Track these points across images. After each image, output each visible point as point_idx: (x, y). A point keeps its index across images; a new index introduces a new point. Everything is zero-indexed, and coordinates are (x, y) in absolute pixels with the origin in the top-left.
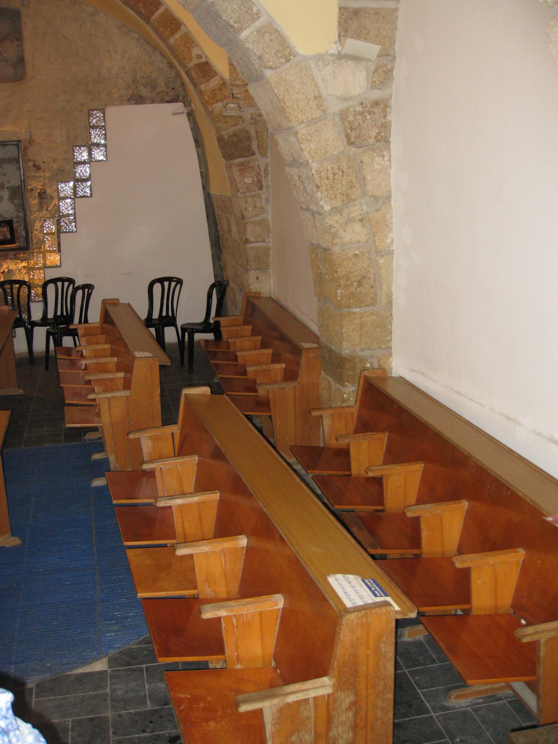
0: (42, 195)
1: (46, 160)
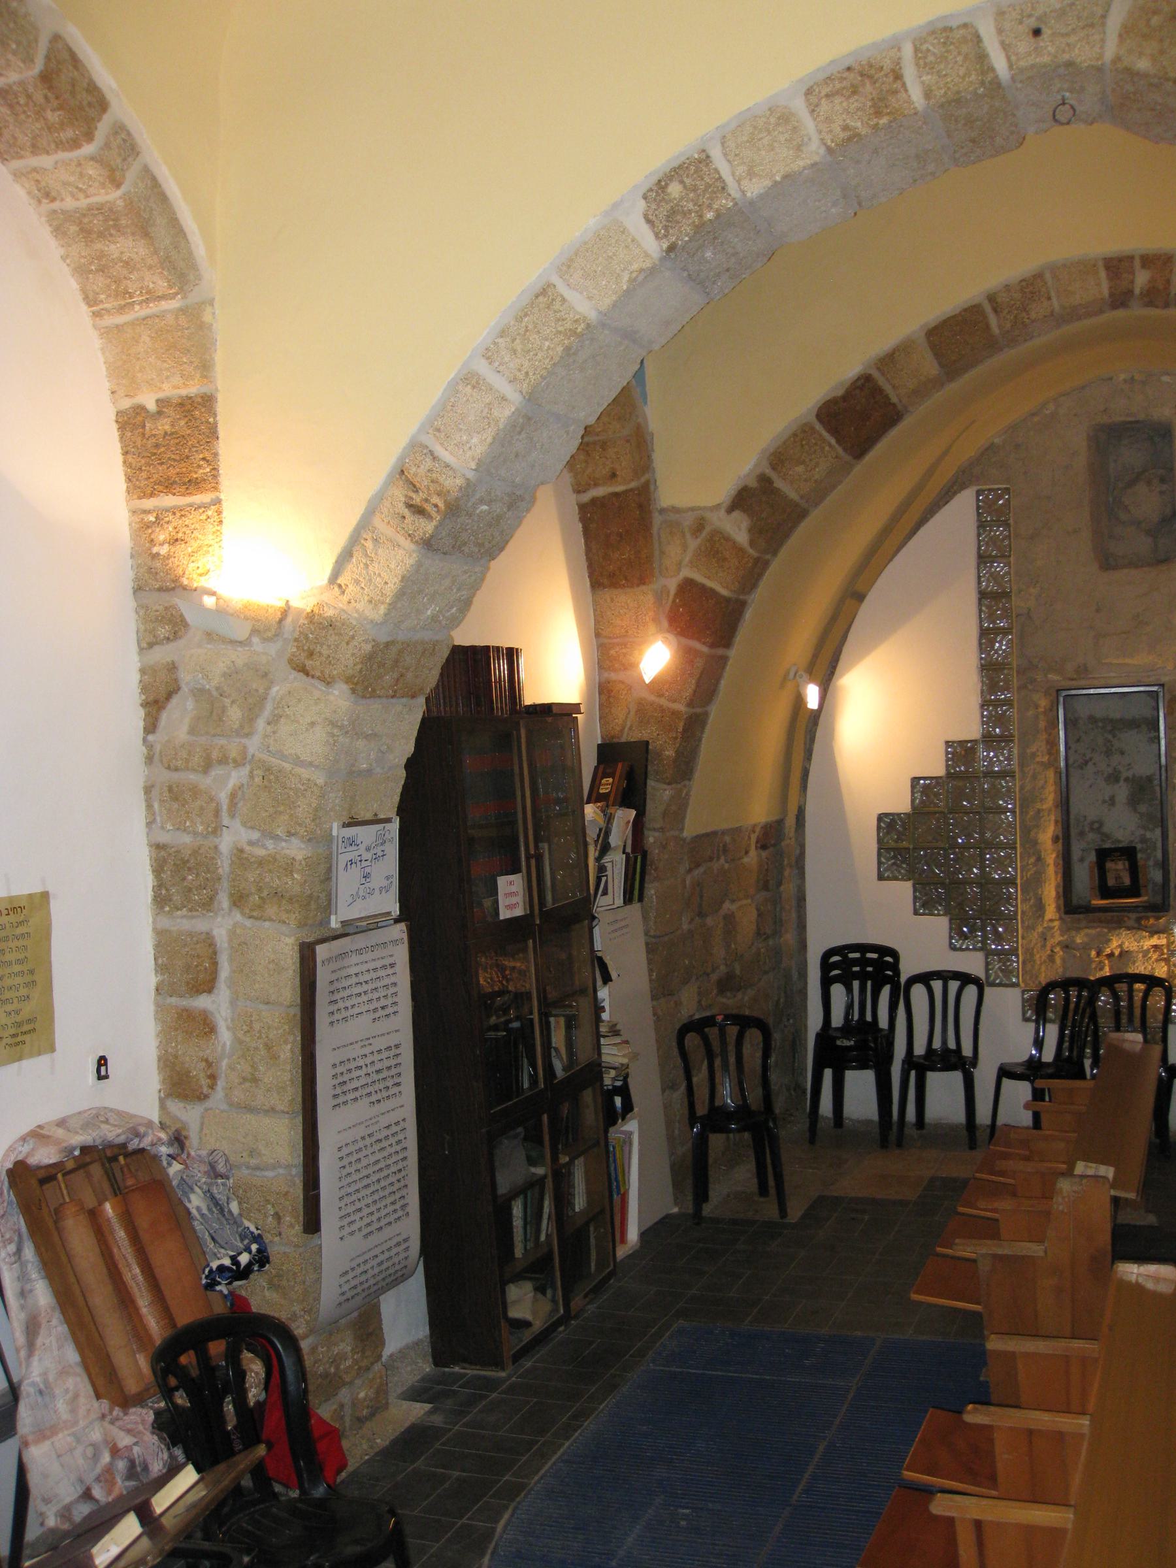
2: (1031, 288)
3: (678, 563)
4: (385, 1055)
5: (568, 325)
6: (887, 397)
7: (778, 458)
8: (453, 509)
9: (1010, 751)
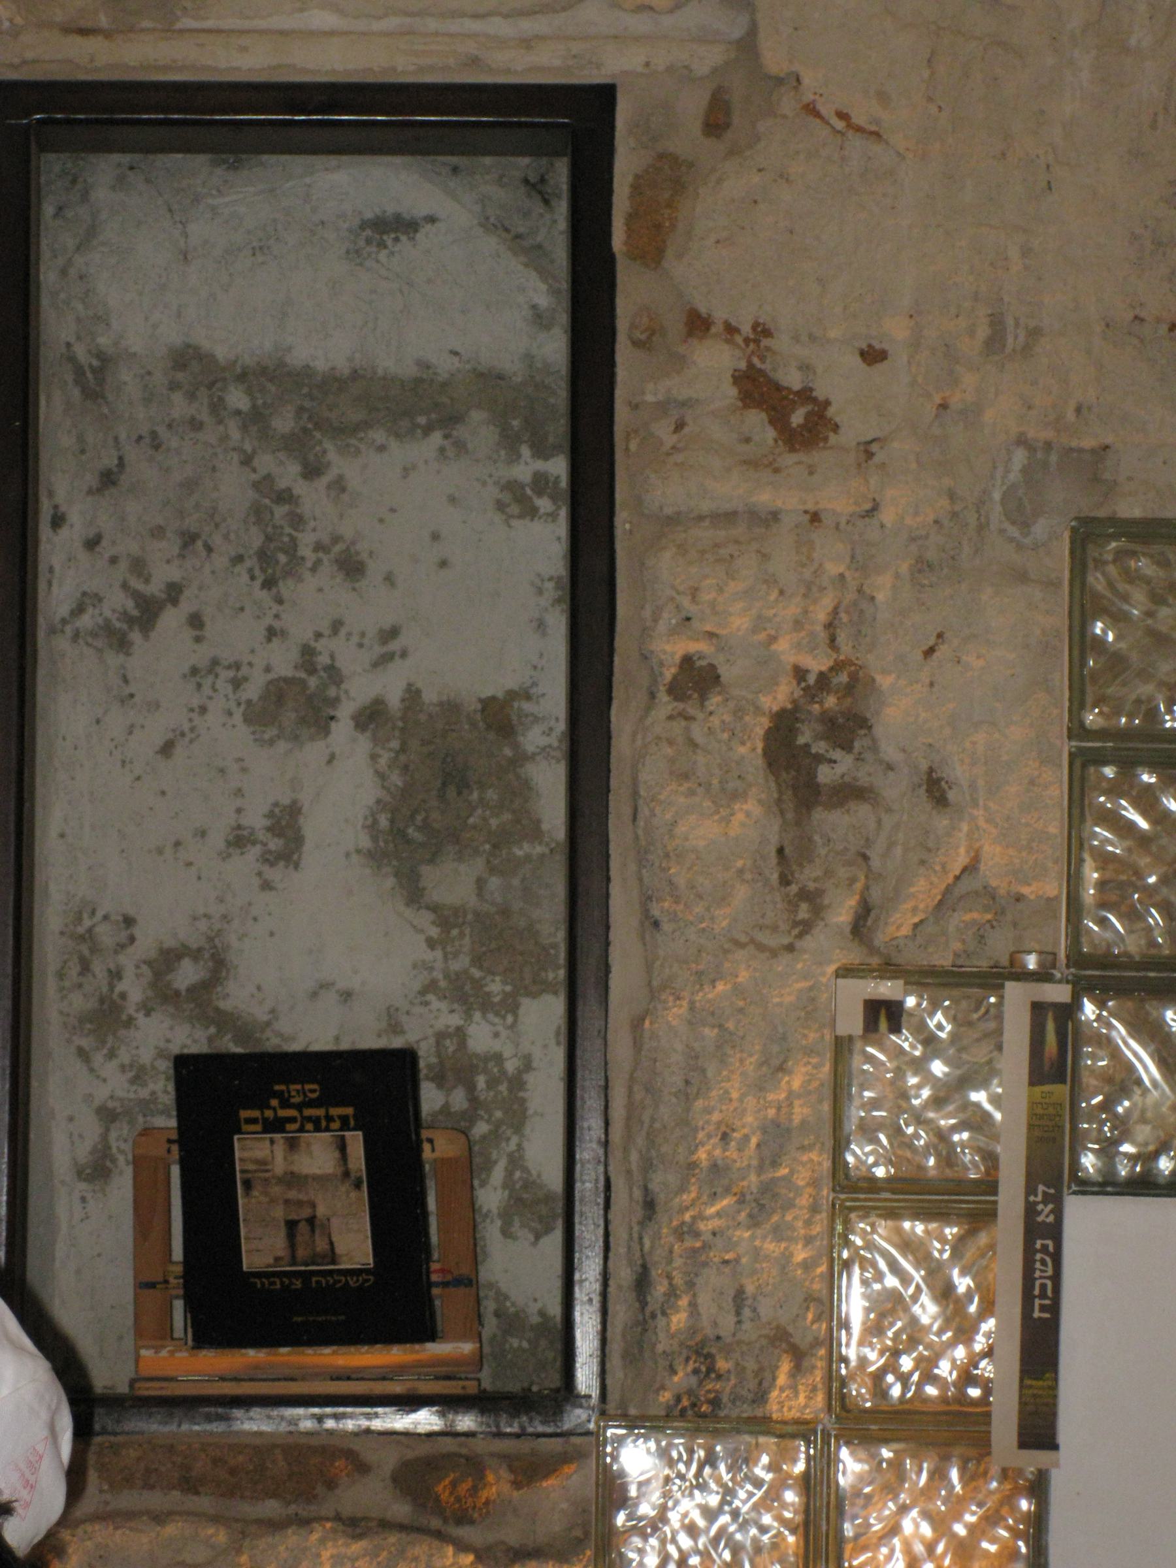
1: (895, 331)
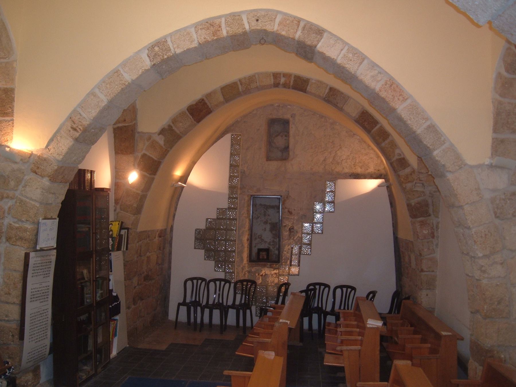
0: (291, 230)
2: (251, 79)
3: (142, 148)
4: (45, 288)
5: (123, 82)
6: (208, 106)
7: (174, 121)
8: (85, 130)
9: (236, 212)
